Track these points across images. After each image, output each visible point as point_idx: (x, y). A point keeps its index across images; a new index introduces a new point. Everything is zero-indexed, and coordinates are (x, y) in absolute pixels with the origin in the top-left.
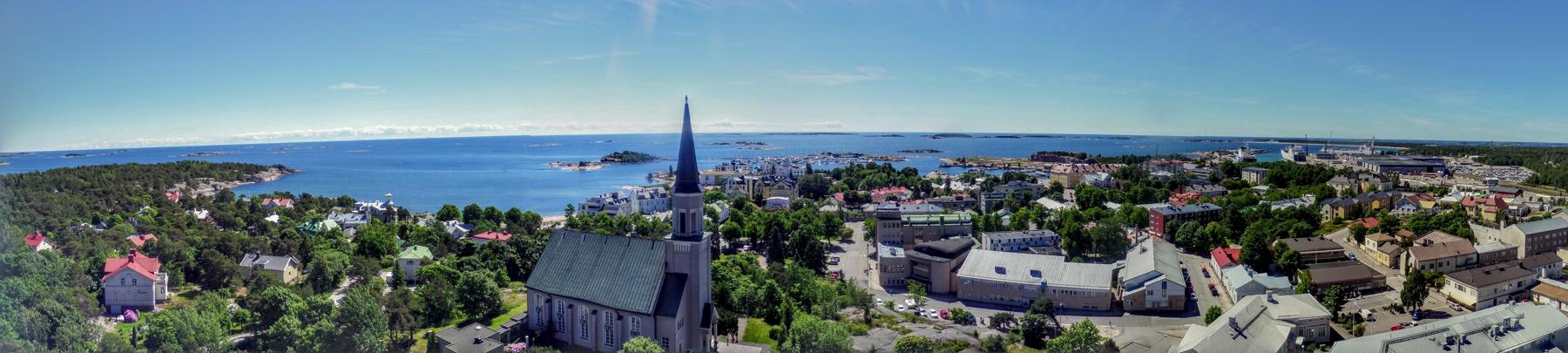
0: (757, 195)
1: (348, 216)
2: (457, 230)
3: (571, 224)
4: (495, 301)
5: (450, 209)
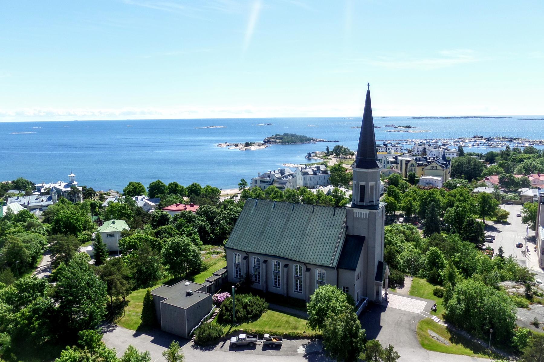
0: (411, 174)
4: (197, 261)
5: (136, 185)
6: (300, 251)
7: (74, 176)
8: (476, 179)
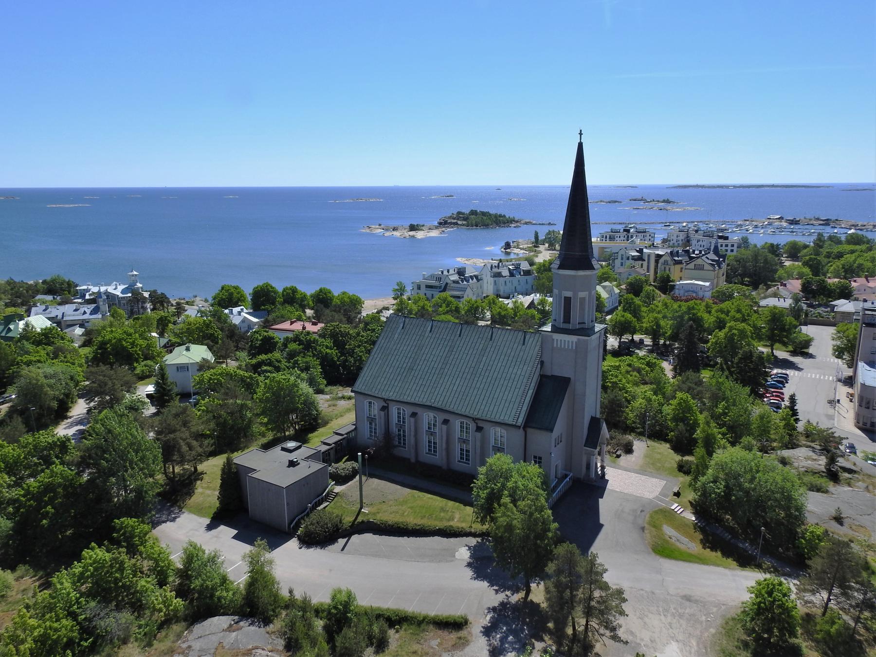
1: (68, 309)
2: (245, 320)
3: (401, 310)
6: (468, 399)
7: (136, 275)
8: (766, 285)
